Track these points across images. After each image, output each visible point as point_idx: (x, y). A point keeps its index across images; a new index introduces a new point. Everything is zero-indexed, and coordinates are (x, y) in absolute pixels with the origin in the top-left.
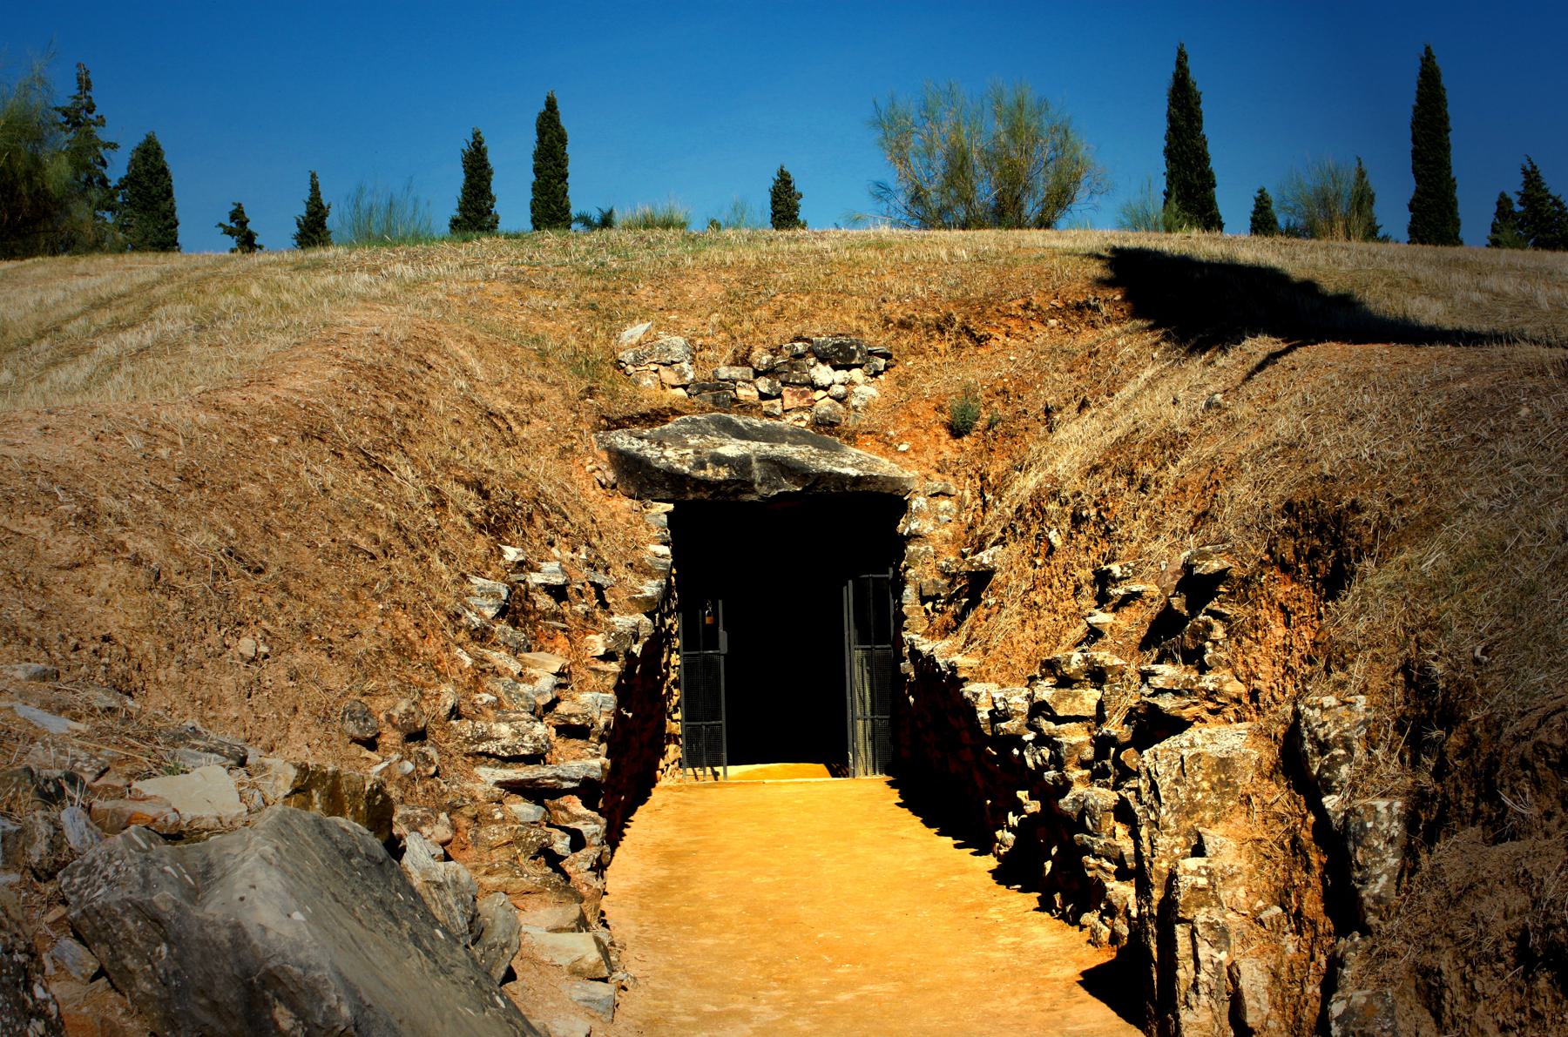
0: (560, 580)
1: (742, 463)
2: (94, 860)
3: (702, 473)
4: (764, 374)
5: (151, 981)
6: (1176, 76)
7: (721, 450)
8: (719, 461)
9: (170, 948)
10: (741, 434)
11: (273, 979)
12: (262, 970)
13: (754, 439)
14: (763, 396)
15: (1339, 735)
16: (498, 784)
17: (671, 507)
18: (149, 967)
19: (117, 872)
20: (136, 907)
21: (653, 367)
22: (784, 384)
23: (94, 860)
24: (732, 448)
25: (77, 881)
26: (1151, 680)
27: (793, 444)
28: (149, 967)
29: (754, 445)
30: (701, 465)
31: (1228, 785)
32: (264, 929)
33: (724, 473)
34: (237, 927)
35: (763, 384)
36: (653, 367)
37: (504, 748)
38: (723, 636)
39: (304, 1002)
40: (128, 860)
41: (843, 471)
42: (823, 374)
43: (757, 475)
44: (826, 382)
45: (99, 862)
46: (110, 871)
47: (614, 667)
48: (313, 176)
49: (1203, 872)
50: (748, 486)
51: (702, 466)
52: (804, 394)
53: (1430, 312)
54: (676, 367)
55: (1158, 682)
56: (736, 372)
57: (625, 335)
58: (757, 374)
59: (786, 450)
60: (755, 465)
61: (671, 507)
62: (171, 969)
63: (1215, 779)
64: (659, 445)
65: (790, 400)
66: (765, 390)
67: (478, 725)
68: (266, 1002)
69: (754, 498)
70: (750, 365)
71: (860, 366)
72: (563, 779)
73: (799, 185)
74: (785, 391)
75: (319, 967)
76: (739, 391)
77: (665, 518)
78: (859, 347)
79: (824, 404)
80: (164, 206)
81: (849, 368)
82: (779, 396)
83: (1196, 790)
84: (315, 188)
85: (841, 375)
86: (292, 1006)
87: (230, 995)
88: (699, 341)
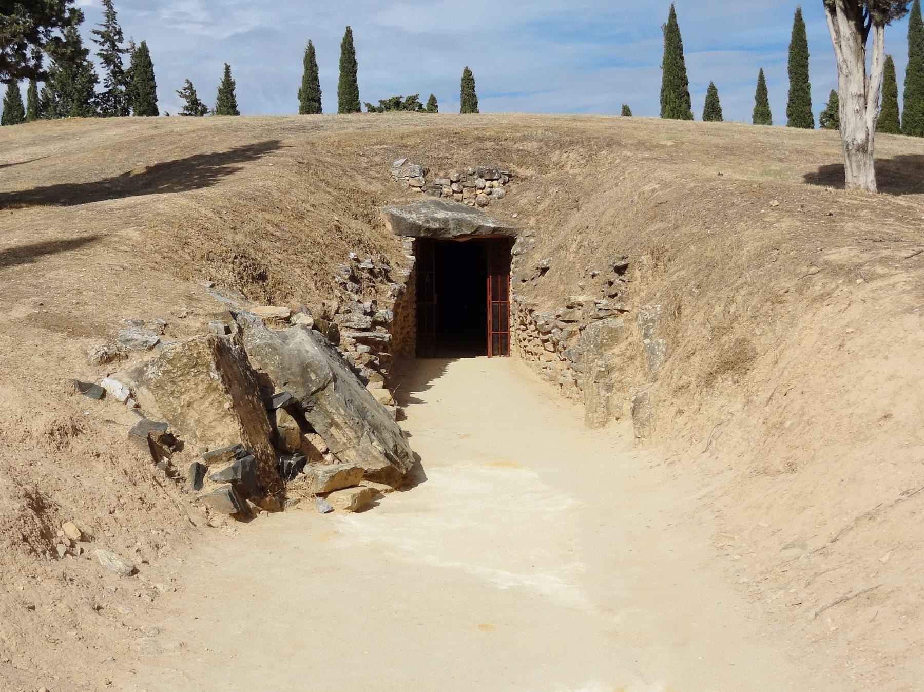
1: (446, 221)
4: (455, 182)
8: (436, 220)
10: (445, 208)
11: (309, 365)
24: (441, 215)
30: (428, 222)
32: (307, 351)
33: (437, 226)
34: (299, 350)
35: (455, 187)
38: (435, 296)
42: (480, 182)
43: (451, 226)
47: (70, 531)
48: (228, 68)
51: (428, 222)
52: (473, 191)
53: (21, 160)
55: (600, 306)
56: (443, 181)
58: (452, 182)
60: (450, 222)
65: (466, 193)
69: (450, 236)
73: (475, 75)
74: (464, 190)
80: (151, 83)
81: (492, 180)
85: (488, 184)
87: (296, 369)
88: (583, 162)
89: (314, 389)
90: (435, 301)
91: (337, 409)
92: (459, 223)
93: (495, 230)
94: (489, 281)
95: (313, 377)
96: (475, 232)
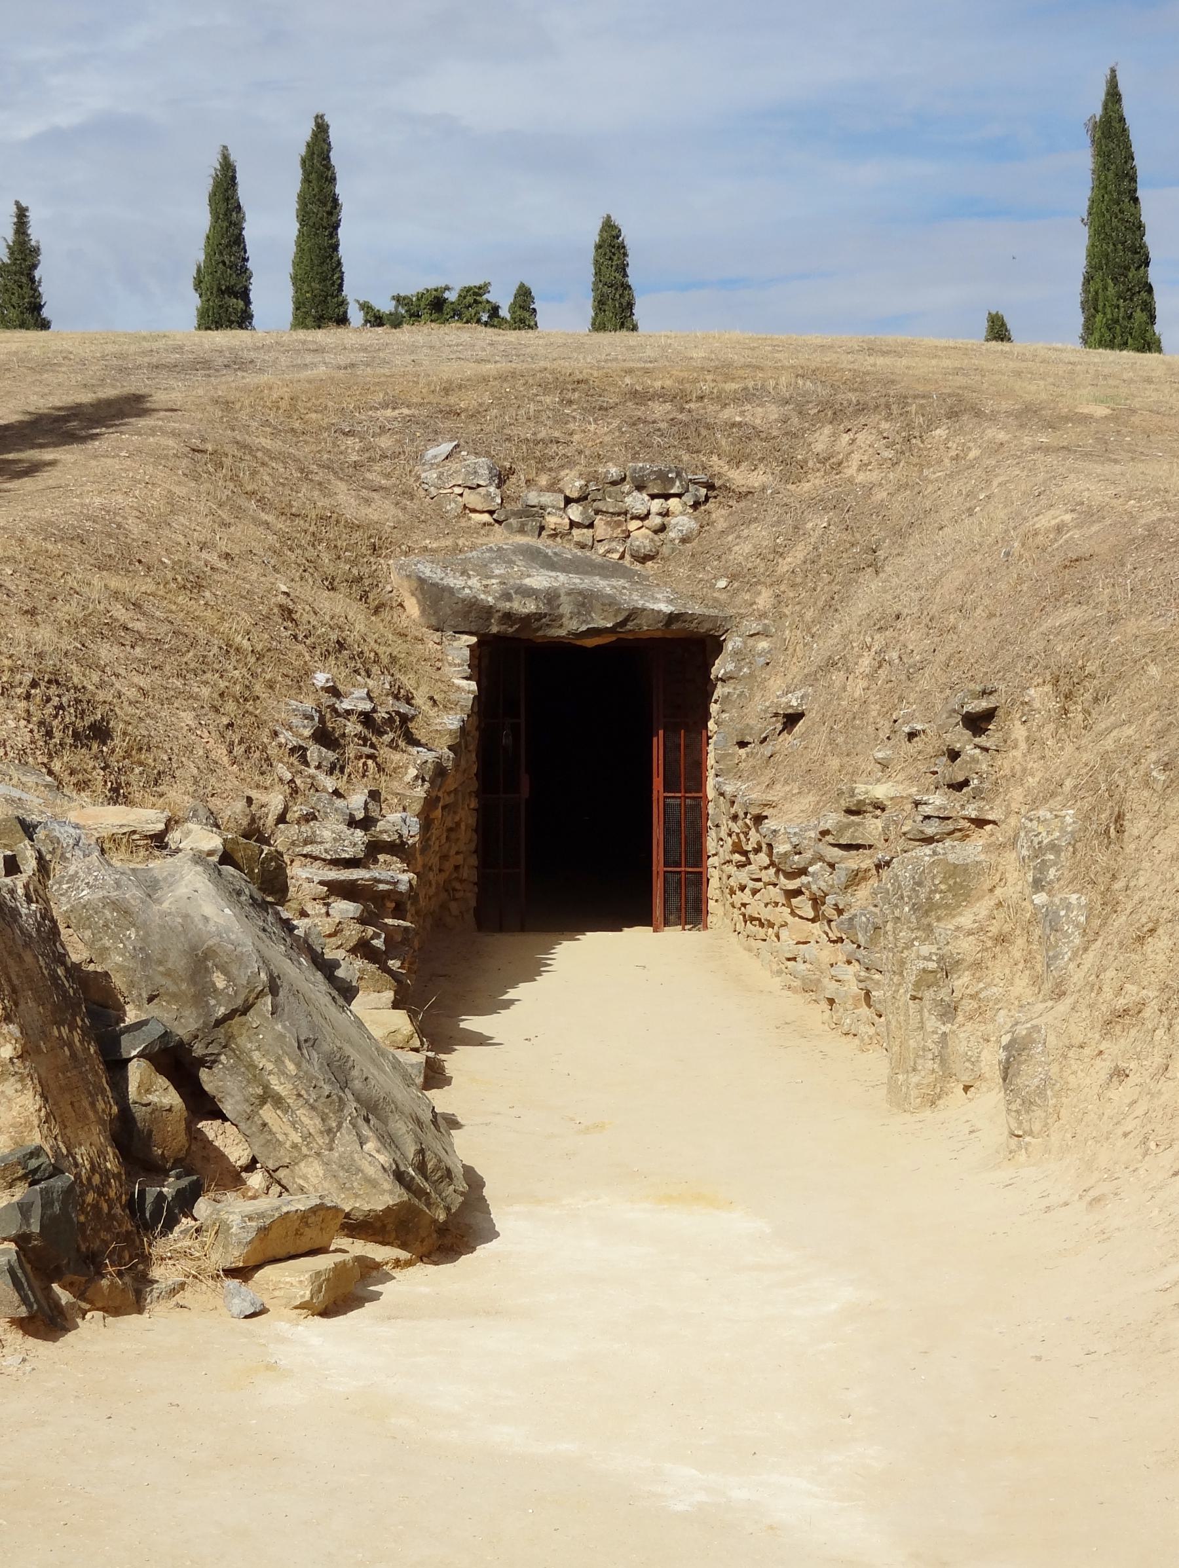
0: (367, 706)
1: (551, 597)
2: (77, 873)
3: (508, 605)
5: (123, 955)
7: (527, 581)
9: (137, 932)
10: (550, 563)
11: (209, 954)
12: (205, 946)
13: (564, 570)
15: (1049, 843)
16: (322, 883)
17: (474, 640)
18: (121, 946)
19: (96, 879)
20: (113, 903)
21: (458, 490)
22: (597, 512)
23: (77, 873)
24: (540, 580)
25: (65, 886)
26: (920, 808)
27: (605, 577)
28: (121, 946)
29: (562, 577)
30: (507, 597)
31: (962, 887)
32: (206, 919)
33: (531, 607)
34: (186, 916)
36: (458, 490)
37: (326, 851)
38: (525, 781)
39: (234, 970)
40: (103, 871)
41: (656, 607)
42: (637, 502)
43: (566, 608)
44: (642, 511)
45: (81, 874)
46: (91, 879)
49: (934, 958)
50: (556, 619)
51: (507, 597)
52: (619, 524)
54: (482, 490)
55: (927, 810)
56: (547, 498)
58: (568, 501)
59: (603, 585)
61: (474, 640)
62: (139, 945)
63: (951, 882)
64: (462, 574)
65: (601, 528)
67: (303, 829)
68: (207, 969)
70: (561, 491)
71: (679, 496)
72: (380, 881)
73: (629, 237)
74: (599, 521)
75: (244, 945)
76: (548, 518)
77: (467, 652)
78: (678, 475)
79: (641, 537)
83: (935, 891)
85: (656, 505)
86: (226, 973)
87: (178, 962)
89: (221, 1011)
90: (525, 792)
91: (279, 1061)
95: (220, 981)
96: (623, 623)
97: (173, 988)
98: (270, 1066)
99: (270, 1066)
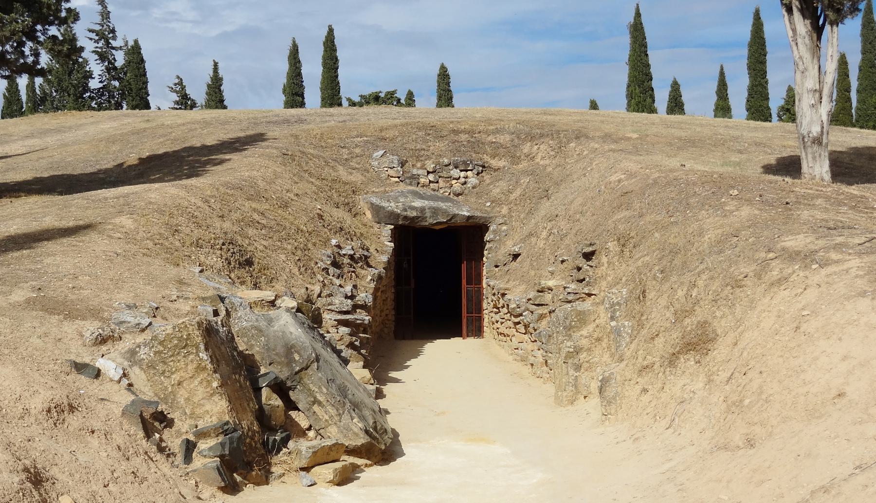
0: (352, 252)
1: (422, 210)
4: (432, 173)
6: (754, 24)
8: (413, 208)
10: (422, 197)
14: (430, 182)
22: (440, 177)
24: (418, 203)
32: (291, 333)
33: (414, 214)
35: (431, 177)
38: (413, 281)
39: (302, 352)
42: (455, 173)
43: (428, 214)
51: (405, 210)
52: (448, 182)
55: (569, 290)
56: (420, 172)
57: (375, 155)
58: (429, 173)
65: (442, 183)
66: (432, 179)
69: (427, 224)
74: (440, 180)
81: (467, 171)
82: (437, 182)
84: (638, 15)
85: (463, 174)
87: (280, 350)
89: (298, 368)
90: (413, 286)
91: (320, 388)
92: (435, 211)
93: (469, 218)
94: (464, 267)
96: (450, 220)
97: (279, 360)
98: (316, 390)
99: (316, 390)
